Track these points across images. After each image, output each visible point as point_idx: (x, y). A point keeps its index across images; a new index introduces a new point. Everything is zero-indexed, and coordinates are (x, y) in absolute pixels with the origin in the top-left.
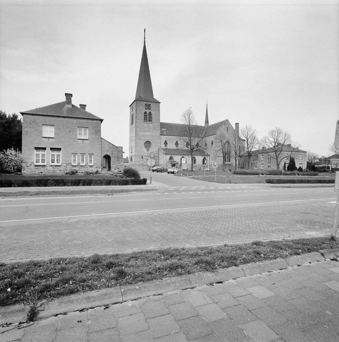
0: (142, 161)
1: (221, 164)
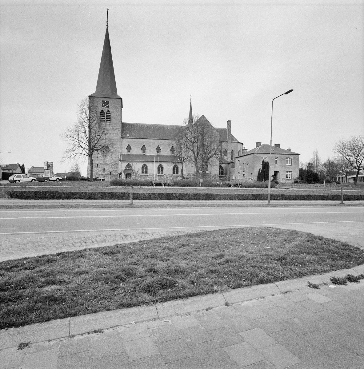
0: (97, 170)
1: (194, 173)
